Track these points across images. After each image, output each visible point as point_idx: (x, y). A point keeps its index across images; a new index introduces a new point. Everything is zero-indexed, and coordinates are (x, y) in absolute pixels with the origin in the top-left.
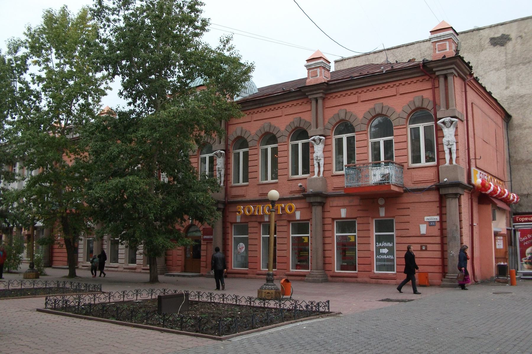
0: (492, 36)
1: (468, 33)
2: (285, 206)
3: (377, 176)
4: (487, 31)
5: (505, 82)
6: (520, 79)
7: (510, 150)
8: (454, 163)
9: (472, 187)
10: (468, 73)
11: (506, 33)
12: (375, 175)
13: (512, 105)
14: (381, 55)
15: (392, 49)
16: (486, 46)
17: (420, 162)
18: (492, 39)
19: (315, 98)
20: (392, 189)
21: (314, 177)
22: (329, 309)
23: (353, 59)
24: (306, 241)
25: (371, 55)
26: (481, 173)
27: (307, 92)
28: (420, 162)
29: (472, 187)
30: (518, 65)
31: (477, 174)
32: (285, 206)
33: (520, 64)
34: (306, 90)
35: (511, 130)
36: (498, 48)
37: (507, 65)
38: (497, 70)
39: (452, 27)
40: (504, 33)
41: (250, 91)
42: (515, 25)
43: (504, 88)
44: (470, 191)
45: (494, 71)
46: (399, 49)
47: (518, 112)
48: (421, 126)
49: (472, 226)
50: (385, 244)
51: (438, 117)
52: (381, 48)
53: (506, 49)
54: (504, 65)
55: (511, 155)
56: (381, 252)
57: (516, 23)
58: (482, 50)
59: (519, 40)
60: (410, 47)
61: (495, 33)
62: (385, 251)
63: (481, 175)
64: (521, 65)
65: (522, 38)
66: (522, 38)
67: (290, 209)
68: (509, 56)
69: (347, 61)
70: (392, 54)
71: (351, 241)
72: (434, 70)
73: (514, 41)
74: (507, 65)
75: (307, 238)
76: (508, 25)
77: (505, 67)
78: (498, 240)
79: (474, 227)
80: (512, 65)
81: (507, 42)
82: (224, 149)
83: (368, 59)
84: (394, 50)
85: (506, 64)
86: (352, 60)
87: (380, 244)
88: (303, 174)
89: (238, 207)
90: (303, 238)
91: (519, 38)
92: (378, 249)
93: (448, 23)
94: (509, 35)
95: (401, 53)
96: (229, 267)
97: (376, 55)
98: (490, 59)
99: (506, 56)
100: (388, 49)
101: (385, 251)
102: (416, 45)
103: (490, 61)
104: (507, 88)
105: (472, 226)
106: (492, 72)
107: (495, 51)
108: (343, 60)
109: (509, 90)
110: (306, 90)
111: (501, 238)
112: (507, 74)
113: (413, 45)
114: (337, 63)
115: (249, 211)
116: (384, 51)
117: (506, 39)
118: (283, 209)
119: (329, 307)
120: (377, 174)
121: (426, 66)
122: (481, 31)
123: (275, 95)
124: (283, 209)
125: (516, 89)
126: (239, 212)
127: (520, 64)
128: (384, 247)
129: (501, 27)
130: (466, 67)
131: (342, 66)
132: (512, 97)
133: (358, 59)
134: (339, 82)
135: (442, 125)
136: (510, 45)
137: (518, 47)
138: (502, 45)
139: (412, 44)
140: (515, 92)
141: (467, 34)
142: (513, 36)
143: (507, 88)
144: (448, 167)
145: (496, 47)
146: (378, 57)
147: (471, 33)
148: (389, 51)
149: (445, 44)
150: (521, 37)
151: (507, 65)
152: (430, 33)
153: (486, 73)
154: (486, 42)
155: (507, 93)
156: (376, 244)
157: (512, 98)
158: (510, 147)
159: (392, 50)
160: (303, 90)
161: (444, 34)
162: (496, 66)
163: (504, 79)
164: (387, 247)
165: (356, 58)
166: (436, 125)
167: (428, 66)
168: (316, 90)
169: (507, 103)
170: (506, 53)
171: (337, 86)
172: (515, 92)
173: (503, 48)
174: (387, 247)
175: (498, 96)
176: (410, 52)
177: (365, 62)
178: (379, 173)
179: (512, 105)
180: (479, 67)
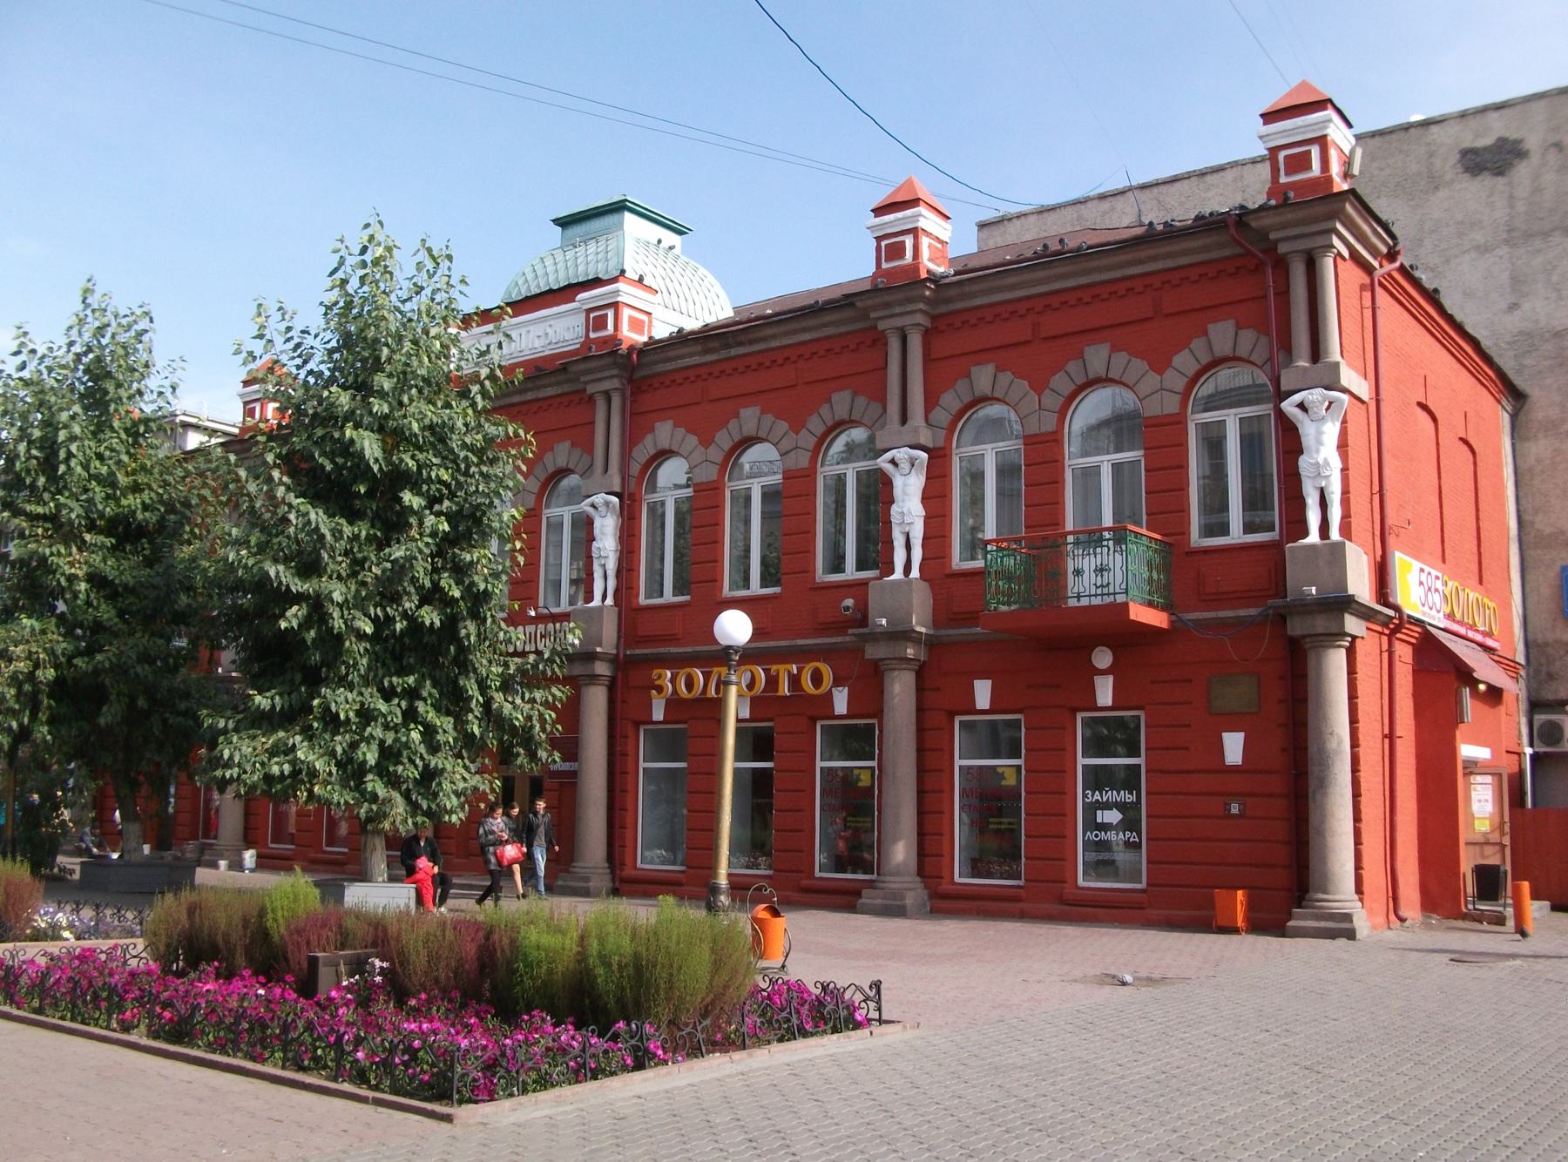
0: (1467, 144)
1: (1394, 136)
2: (800, 670)
3: (1086, 576)
4: (1452, 130)
5: (1509, 290)
6: (1555, 278)
7: (1523, 502)
8: (1335, 535)
9: (1391, 613)
10: (1384, 250)
11: (1513, 135)
12: (1078, 572)
13: (1528, 362)
14: (1119, 203)
15: (1157, 184)
16: (1448, 177)
17: (1228, 534)
18: (1466, 153)
19: (897, 328)
20: (1132, 617)
21: (892, 578)
22: (879, 1010)
23: (1035, 216)
24: (865, 780)
25: (1089, 204)
26: (1422, 570)
27: (875, 308)
28: (1228, 534)
29: (1391, 613)
30: (1546, 234)
31: (1409, 571)
32: (800, 670)
33: (1554, 230)
34: (870, 302)
35: (1527, 439)
36: (1486, 181)
37: (1515, 236)
38: (1482, 249)
39: (1330, 101)
40: (1506, 134)
41: (706, 311)
42: (1539, 110)
43: (1504, 305)
44: (1385, 625)
45: (1474, 255)
46: (1178, 185)
47: (1548, 381)
48: (1232, 417)
49: (1391, 737)
50: (1111, 795)
51: (1283, 388)
52: (1120, 183)
53: (1510, 184)
54: (1505, 236)
55: (1526, 517)
56: (1099, 820)
57: (1542, 103)
58: (1437, 188)
59: (1553, 157)
60: (1209, 178)
61: (1477, 136)
62: (1113, 817)
63: (1424, 576)
64: (1557, 233)
65: (1561, 151)
66: (1561, 151)
67: (817, 679)
68: (1521, 207)
69: (1017, 223)
70: (1156, 202)
71: (1004, 783)
72: (1273, 236)
73: (1535, 159)
74: (1515, 236)
75: (869, 771)
76: (1518, 108)
77: (1506, 242)
78: (1479, 787)
79: (1398, 741)
80: (1529, 236)
81: (1516, 162)
82: (617, 489)
83: (1080, 218)
84: (1163, 189)
85: (1509, 231)
86: (1032, 219)
87: (1097, 796)
88: (857, 570)
89: (656, 672)
90: (1000, 770)
91: (1552, 150)
92: (1091, 809)
93: (1320, 87)
94: (1521, 141)
95: (1183, 199)
96: (628, 861)
97: (1106, 205)
98: (1459, 217)
99: (1512, 207)
100: (1143, 187)
101: (1113, 817)
102: (1229, 175)
103: (1462, 222)
104: (1513, 307)
105: (1391, 737)
106: (1467, 257)
107: (1476, 193)
108: (1002, 220)
109: (1519, 312)
110: (870, 302)
111: (1489, 779)
112: (1513, 264)
113: (1221, 174)
114: (985, 231)
115: (690, 685)
116: (1131, 193)
117: (1509, 152)
118: (795, 681)
119: (879, 1002)
120: (1086, 569)
121: (1247, 225)
122: (1434, 129)
123: (775, 319)
124: (795, 681)
125: (1540, 310)
126: (660, 689)
127: (1554, 230)
128: (1107, 806)
129: (1494, 115)
130: (1375, 231)
131: (999, 238)
132: (1529, 335)
133: (1051, 217)
134: (980, 277)
135: (1297, 411)
136: (1522, 172)
137: (1549, 177)
138: (1500, 171)
139: (1219, 169)
140: (1537, 321)
141: (1387, 138)
142: (1533, 142)
143: (1513, 307)
144: (1312, 547)
145: (1480, 178)
146: (1113, 209)
147: (1401, 135)
148: (1147, 192)
149: (1309, 152)
150: (1558, 146)
151: (1514, 234)
152: (1261, 121)
153: (1447, 261)
154: (1448, 164)
155: (1513, 322)
156: (1084, 796)
157: (1528, 339)
158: (1521, 494)
159: (1155, 190)
160: (859, 304)
161: (1306, 123)
162: (1479, 237)
163: (1505, 277)
164: (1121, 806)
165: (1045, 215)
166: (1281, 416)
167: (1254, 224)
168: (900, 303)
169: (1511, 353)
170: (1511, 197)
171: (967, 289)
172: (1537, 321)
173: (1501, 180)
174: (1121, 806)
175: (1485, 333)
176: (1210, 194)
177: (1073, 225)
178: (1093, 567)
179: (1528, 362)
180: (1426, 241)
